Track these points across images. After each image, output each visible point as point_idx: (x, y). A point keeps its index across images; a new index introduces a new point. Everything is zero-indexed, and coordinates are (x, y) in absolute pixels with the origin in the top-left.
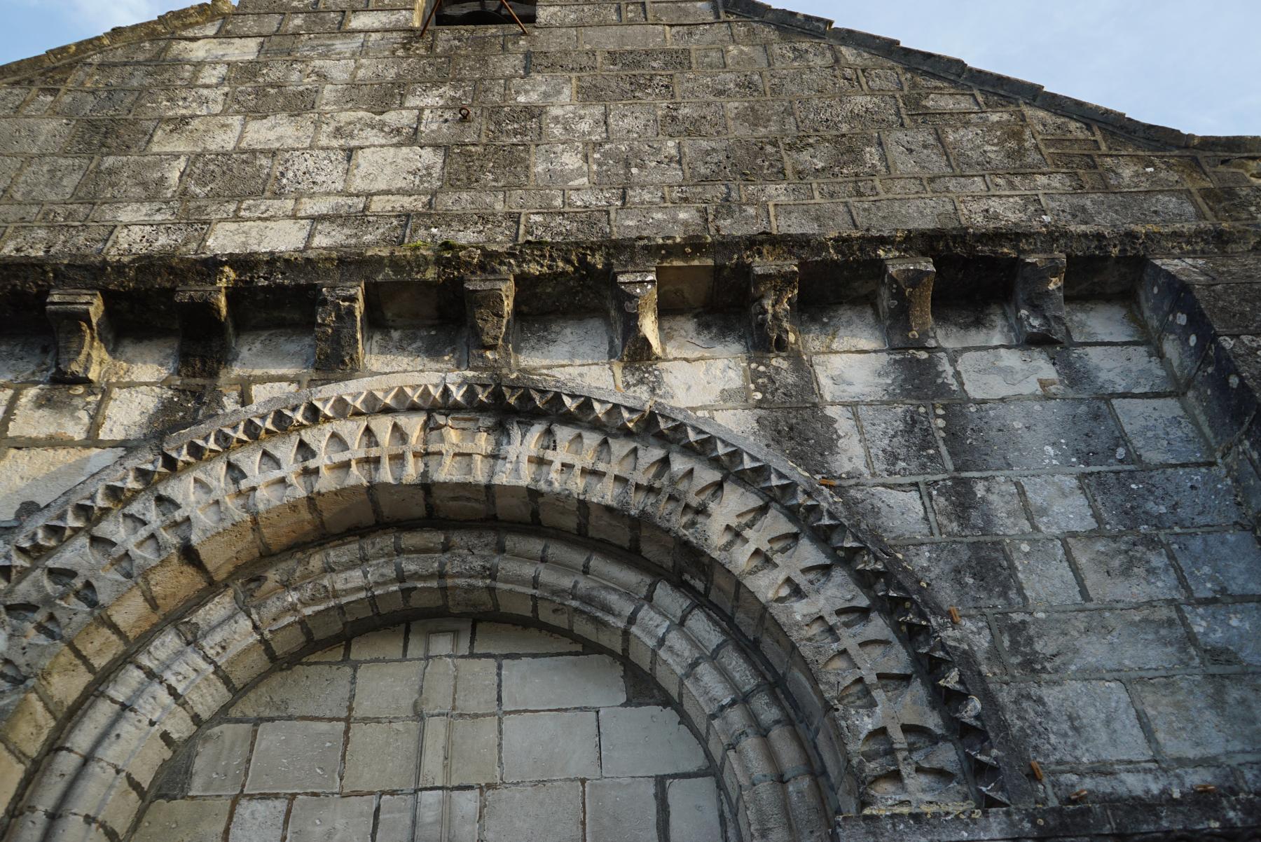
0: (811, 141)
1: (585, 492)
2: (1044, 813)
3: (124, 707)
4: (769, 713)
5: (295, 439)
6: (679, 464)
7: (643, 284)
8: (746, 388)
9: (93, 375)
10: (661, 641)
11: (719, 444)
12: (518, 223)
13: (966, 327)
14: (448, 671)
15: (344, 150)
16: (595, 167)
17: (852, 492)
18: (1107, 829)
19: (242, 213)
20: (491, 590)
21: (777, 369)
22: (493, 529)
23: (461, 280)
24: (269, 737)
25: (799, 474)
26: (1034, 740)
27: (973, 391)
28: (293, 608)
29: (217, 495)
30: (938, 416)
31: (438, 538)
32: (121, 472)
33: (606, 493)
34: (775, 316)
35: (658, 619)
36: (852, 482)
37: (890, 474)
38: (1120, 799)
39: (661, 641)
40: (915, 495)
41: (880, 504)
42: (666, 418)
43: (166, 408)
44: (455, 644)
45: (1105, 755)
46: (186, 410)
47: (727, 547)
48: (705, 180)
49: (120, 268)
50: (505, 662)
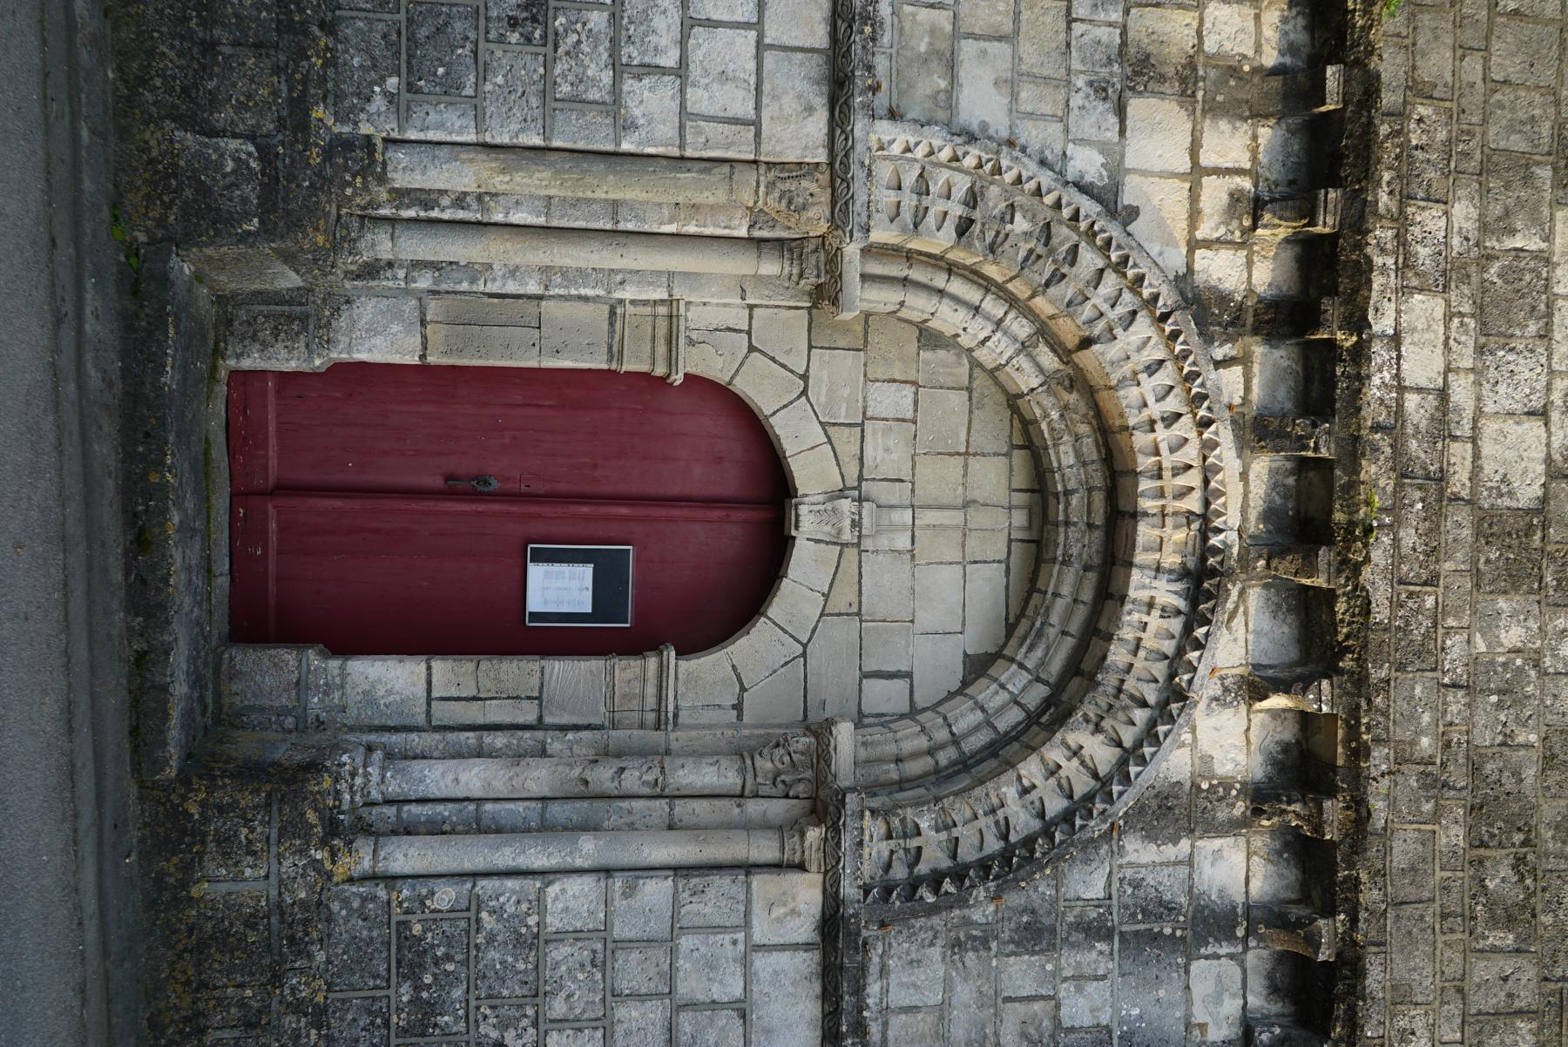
0: (1528, 881)
1: (1120, 639)
2: (858, 923)
3: (977, 309)
4: (944, 758)
5: (1183, 410)
6: (1140, 715)
7: (1323, 699)
8: (1213, 777)
9: (1259, 231)
10: (1003, 686)
11: (1153, 749)
12: (1425, 584)
13: (1270, 977)
14: (999, 527)
15: (1545, 406)
16: (1501, 659)
17: (1106, 847)
18: (846, 960)
19: (1456, 321)
20: (1054, 560)
21: (1233, 805)
22: (1105, 562)
23: (1330, 542)
24: (958, 400)
25: (1121, 808)
26: (905, 931)
27: (1196, 966)
28: (1046, 415)
29: (1135, 357)
30: (1174, 930)
31: (1099, 520)
32: (1156, 283)
33: (1118, 655)
34: (1284, 812)
35: (1020, 686)
36: (1115, 848)
37: (1121, 880)
38: (864, 977)
39: (1003, 686)
40: (1101, 895)
41: (1094, 865)
42: (1182, 709)
43: (1223, 298)
44: (1020, 529)
45: (893, 976)
46: (1221, 315)
47: (1064, 743)
48: (1475, 769)
49: (1360, 246)
50: (1003, 566)
